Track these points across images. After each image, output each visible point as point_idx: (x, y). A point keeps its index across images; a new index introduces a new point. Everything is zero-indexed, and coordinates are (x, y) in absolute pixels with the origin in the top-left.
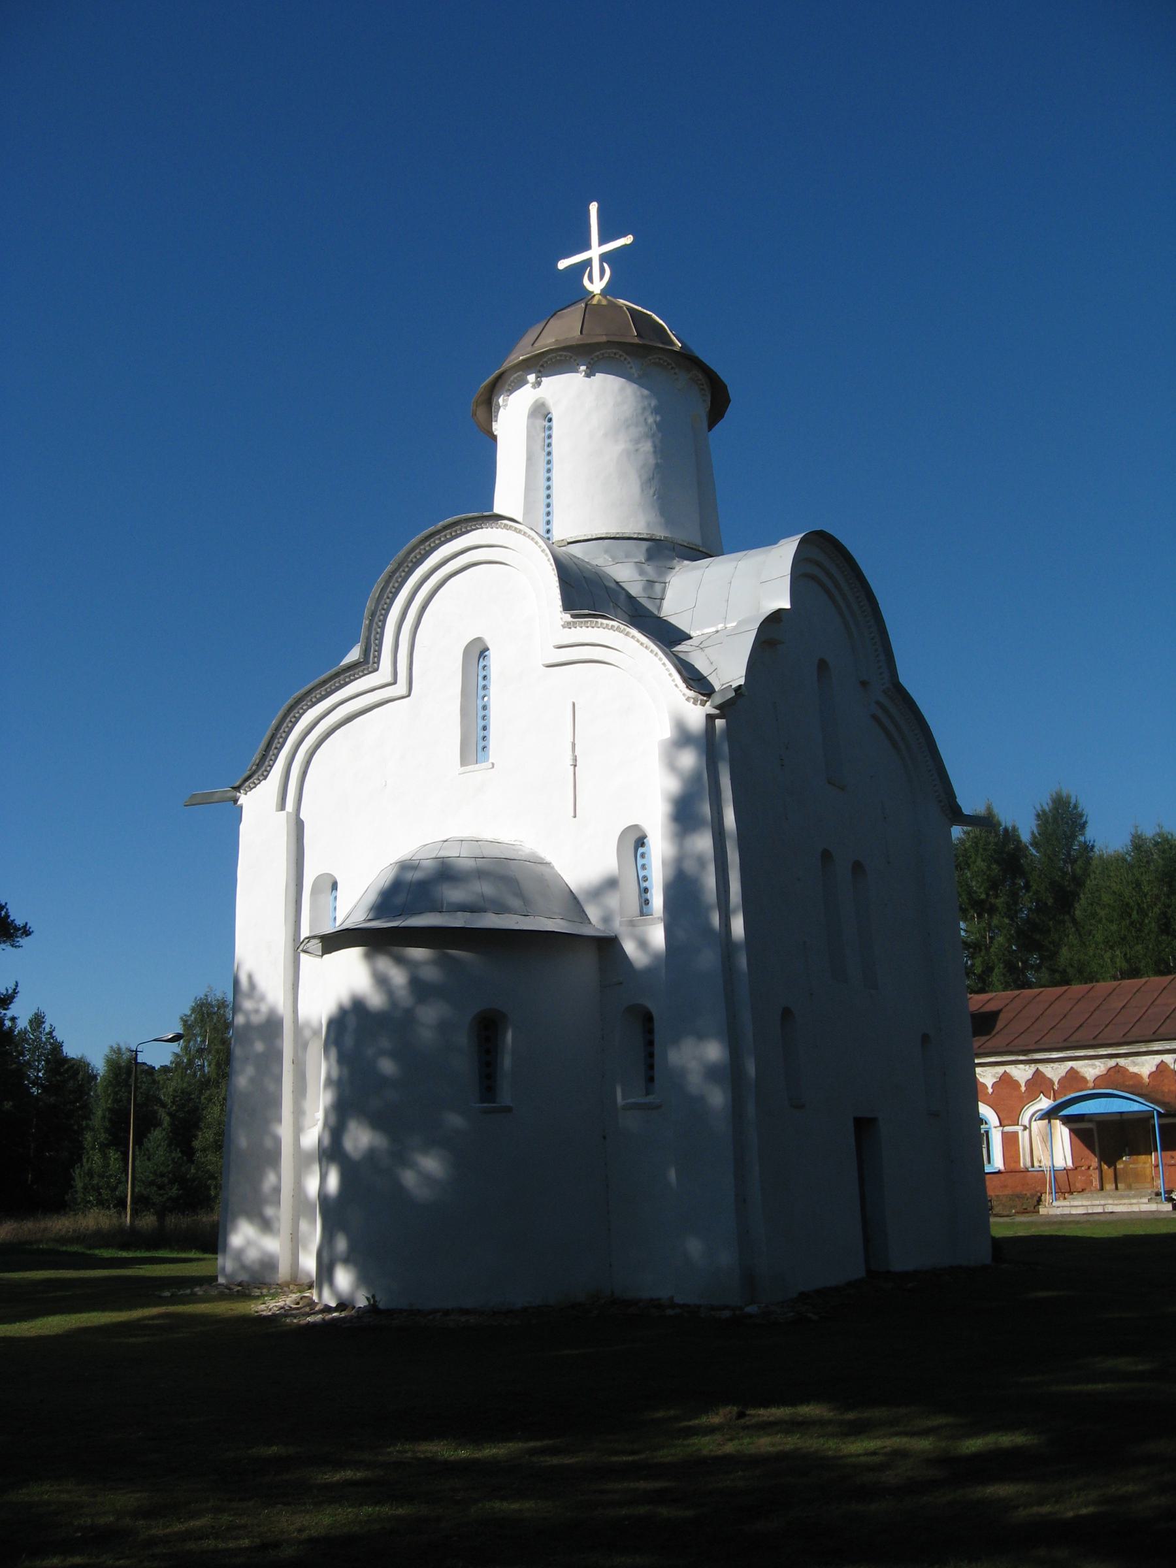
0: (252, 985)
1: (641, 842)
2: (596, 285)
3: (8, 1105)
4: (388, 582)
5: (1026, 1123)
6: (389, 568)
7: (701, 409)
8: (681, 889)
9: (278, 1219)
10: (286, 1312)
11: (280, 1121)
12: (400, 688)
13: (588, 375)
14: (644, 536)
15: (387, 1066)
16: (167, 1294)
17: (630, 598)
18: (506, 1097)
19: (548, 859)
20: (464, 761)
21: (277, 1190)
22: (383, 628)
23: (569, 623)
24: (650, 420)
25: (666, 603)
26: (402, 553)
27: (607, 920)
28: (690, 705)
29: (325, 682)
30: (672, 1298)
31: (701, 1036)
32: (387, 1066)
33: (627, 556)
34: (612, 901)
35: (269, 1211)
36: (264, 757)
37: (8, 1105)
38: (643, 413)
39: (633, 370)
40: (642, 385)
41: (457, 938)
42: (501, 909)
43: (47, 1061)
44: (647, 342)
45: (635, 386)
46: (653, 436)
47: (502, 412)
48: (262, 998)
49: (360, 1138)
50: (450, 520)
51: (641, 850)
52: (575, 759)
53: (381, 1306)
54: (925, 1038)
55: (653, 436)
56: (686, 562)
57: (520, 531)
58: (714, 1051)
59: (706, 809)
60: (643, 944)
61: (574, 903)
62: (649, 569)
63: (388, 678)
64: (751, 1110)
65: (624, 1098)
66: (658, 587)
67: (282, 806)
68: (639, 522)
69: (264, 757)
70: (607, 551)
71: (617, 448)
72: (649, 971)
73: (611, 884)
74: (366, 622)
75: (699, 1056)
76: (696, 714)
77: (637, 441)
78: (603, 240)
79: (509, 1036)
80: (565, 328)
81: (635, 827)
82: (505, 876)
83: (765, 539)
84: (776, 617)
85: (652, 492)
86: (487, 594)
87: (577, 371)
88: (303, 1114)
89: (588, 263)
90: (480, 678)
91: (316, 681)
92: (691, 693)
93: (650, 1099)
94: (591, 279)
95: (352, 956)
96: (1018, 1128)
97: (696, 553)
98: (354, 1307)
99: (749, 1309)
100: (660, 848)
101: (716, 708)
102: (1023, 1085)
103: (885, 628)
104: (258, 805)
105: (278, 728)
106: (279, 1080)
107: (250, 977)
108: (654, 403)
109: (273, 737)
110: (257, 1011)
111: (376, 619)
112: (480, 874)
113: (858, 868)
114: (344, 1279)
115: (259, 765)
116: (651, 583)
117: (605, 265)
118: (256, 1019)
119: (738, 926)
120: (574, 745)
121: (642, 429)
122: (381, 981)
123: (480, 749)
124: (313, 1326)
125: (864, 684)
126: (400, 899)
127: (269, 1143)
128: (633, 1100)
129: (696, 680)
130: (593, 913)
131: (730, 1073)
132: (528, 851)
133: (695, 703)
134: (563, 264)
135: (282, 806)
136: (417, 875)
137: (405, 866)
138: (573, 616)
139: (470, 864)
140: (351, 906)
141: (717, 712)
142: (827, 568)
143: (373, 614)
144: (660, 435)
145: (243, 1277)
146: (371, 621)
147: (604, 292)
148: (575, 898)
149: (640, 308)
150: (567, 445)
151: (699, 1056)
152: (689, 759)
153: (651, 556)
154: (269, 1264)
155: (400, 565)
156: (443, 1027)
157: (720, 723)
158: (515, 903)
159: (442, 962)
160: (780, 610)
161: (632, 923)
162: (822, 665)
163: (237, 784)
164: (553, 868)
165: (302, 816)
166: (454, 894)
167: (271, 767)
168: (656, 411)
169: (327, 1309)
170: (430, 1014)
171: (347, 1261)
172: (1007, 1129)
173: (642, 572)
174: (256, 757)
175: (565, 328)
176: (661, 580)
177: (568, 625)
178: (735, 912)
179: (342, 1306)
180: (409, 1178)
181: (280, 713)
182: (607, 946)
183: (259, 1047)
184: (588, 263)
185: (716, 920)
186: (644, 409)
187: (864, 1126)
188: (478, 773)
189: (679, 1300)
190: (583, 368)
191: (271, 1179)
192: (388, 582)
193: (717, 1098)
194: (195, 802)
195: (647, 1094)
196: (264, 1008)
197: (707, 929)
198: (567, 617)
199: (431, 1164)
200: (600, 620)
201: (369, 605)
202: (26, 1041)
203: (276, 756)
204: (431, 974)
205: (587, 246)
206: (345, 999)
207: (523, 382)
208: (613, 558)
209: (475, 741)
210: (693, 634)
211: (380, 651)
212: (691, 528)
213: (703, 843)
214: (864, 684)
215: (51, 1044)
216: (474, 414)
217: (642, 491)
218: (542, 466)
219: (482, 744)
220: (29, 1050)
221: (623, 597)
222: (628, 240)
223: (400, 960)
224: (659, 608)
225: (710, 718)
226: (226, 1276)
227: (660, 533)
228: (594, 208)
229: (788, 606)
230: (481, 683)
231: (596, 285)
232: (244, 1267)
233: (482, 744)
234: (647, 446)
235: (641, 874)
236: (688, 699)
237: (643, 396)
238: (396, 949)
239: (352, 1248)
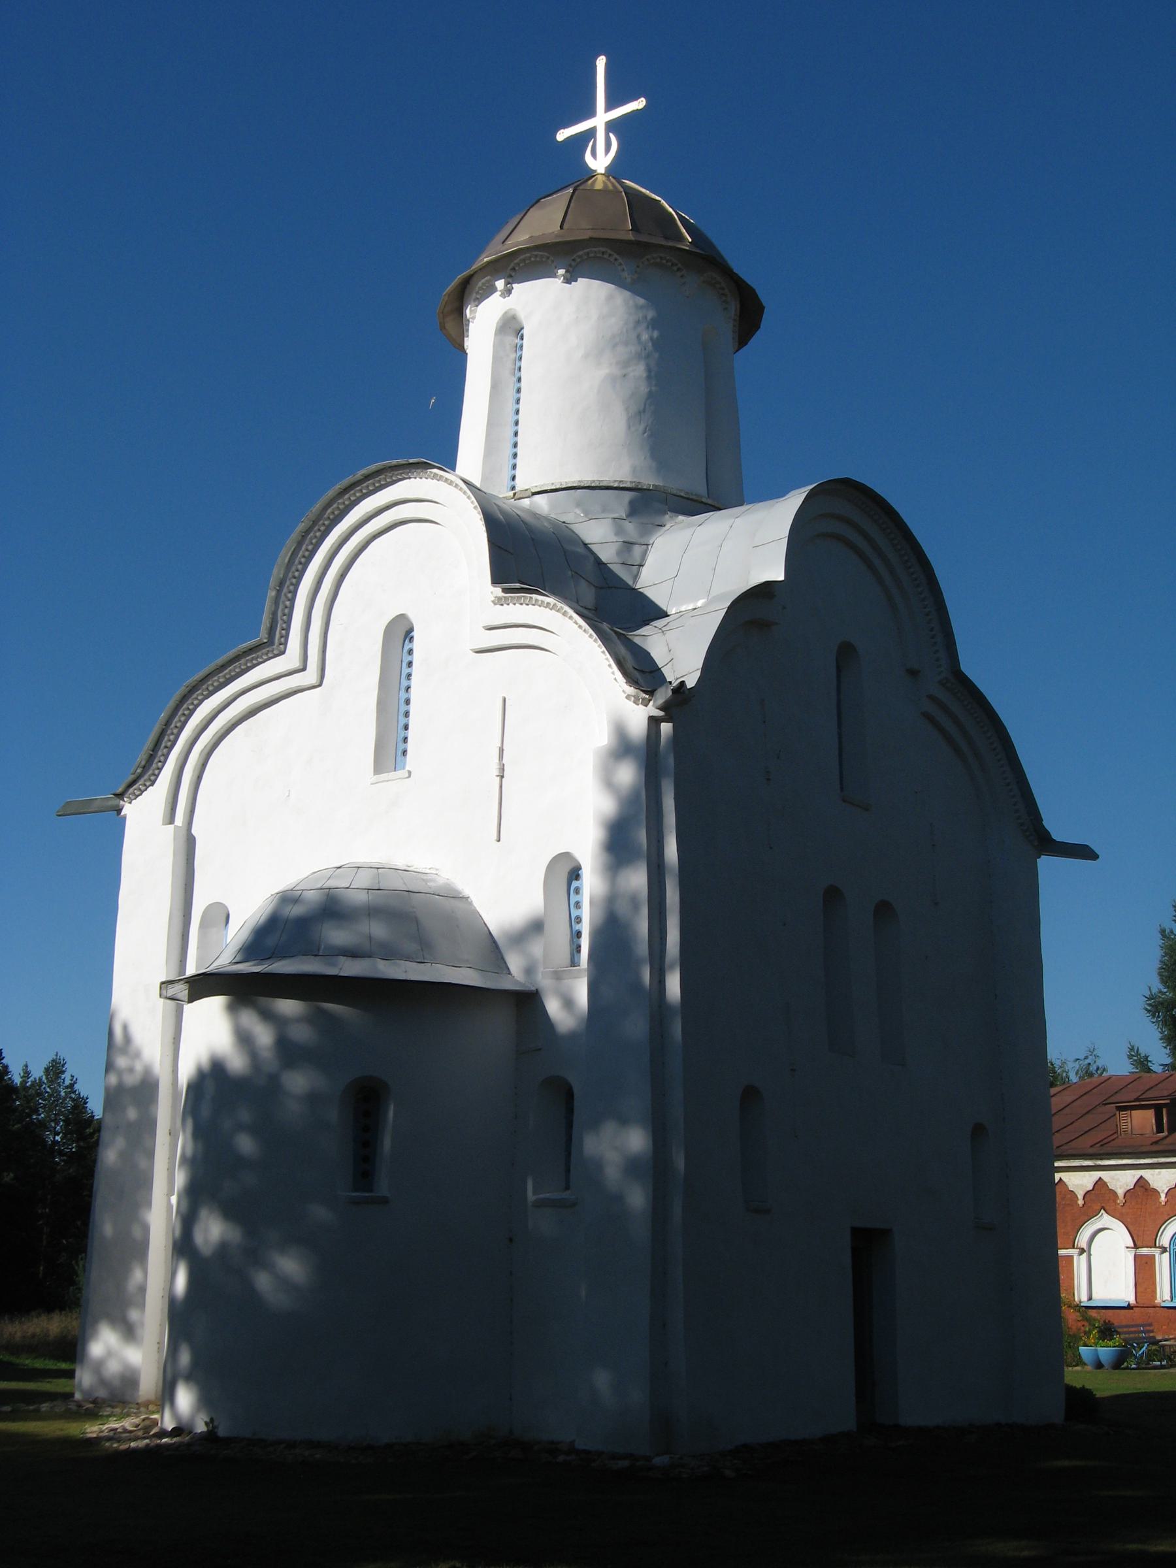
1: (575, 874)
2: (599, 160)
3: (9, 1177)
4: (300, 544)
5: (1084, 1245)
6: (301, 527)
7: (722, 321)
8: (611, 937)
9: (142, 1324)
10: (115, 1436)
11: (149, 1204)
12: (310, 676)
13: (568, 280)
14: (628, 485)
15: (246, 1144)
16: (7, 1408)
17: (600, 564)
18: (383, 1186)
19: (467, 891)
20: (378, 768)
21: (142, 1289)
22: (293, 600)
23: (499, 599)
24: (645, 337)
25: (645, 571)
26: (318, 506)
27: (529, 971)
29: (223, 667)
30: (573, 1442)
31: (624, 1121)
32: (246, 1144)
33: (604, 511)
34: (537, 948)
35: (134, 1315)
36: (151, 758)
37: (9, 1177)
38: (635, 328)
39: (625, 274)
41: (343, 985)
42: (389, 953)
43: (67, 1122)
44: (644, 238)
45: (627, 294)
46: (648, 356)
48: (137, 1055)
49: (213, 1230)
51: (575, 884)
52: (502, 769)
53: (222, 1432)
54: (978, 1130)
56: (681, 518)
57: (451, 483)
58: (636, 1140)
60: (568, 1003)
61: (492, 951)
62: (631, 527)
64: (677, 1211)
65: (534, 1193)
66: (637, 550)
67: (170, 818)
68: (621, 471)
69: (151, 758)
70: (578, 505)
72: (573, 1036)
73: (536, 927)
74: (272, 593)
75: (618, 1144)
76: (637, 716)
77: (625, 364)
78: (611, 105)
79: (391, 1114)
80: (544, 221)
81: (566, 856)
82: (408, 913)
83: (777, 492)
84: (765, 591)
85: (642, 427)
87: (554, 276)
88: (158, 1194)
89: (591, 133)
90: (404, 665)
92: (631, 690)
93: (566, 1195)
94: (594, 154)
95: (213, 1007)
96: (1073, 1252)
98: (190, 1432)
99: (658, 1461)
100: (592, 883)
101: (660, 709)
102: (1080, 1197)
103: (943, 601)
104: (144, 815)
105: (168, 723)
106: (151, 1155)
107: (125, 1028)
108: (651, 314)
109: (162, 734)
110: (131, 1070)
111: (285, 590)
112: (373, 911)
113: (884, 910)
114: (185, 1399)
115: (145, 768)
116: (628, 544)
117: (611, 135)
118: (130, 1080)
119: (673, 985)
120: (501, 750)
121: (634, 348)
122: (243, 1038)
123: (400, 752)
124: (135, 1451)
125: (913, 673)
126: (271, 941)
127: (137, 1232)
128: (548, 1195)
129: (642, 673)
130: (515, 963)
131: (655, 1169)
133: (636, 702)
134: (562, 135)
135: (170, 818)
136: (296, 911)
137: (287, 898)
138: (505, 590)
139: (361, 898)
141: (661, 713)
142: (851, 528)
143: (281, 584)
144: (656, 355)
145: (102, 1393)
146: (279, 592)
147: (611, 171)
148: (495, 942)
150: (546, 372)
151: (618, 1144)
152: (627, 774)
154: (130, 1379)
156: (312, 1099)
157: (666, 728)
158: (411, 947)
159: (317, 1019)
160: (768, 585)
161: (558, 976)
162: (846, 652)
163: (120, 790)
164: (471, 903)
165: (194, 832)
166: (337, 936)
167: (160, 769)
168: (654, 324)
169: (163, 1433)
170: (298, 1082)
171: (189, 1378)
172: (1144, 1251)
173: (619, 531)
174: (142, 758)
175: (544, 221)
176: (643, 541)
177: (499, 601)
178: (672, 967)
179: (177, 1431)
180: (263, 1281)
181: (171, 704)
183: (132, 1114)
184: (591, 133)
185: (646, 975)
186: (638, 322)
187: (868, 1244)
188: (393, 783)
189: (580, 1445)
190: (561, 272)
191: (137, 1275)
192: (300, 544)
193: (637, 1198)
194: (70, 810)
195: (567, 1188)
196: (139, 1067)
197: (637, 986)
198: (498, 591)
199: (291, 1266)
200: (534, 596)
201: (277, 573)
202: (40, 1094)
203: (166, 756)
204: (302, 1034)
205: (590, 112)
206: (205, 1061)
207: (490, 290)
208: (586, 513)
209: (391, 748)
210: (672, 611)
212: (688, 476)
213: (637, 879)
214: (913, 673)
215: (73, 1100)
216: (443, 327)
218: (511, 394)
219: (401, 746)
220: (44, 1107)
221: (592, 559)
222: (639, 104)
223: (267, 1016)
224: (636, 577)
225: (654, 722)
226: (82, 1391)
228: (601, 63)
229: (777, 573)
230: (405, 671)
231: (599, 160)
232: (103, 1382)
233: (401, 746)
234: (639, 370)
235: (574, 913)
236: (628, 697)
237: (639, 308)
238: (264, 1001)
239: (195, 1363)
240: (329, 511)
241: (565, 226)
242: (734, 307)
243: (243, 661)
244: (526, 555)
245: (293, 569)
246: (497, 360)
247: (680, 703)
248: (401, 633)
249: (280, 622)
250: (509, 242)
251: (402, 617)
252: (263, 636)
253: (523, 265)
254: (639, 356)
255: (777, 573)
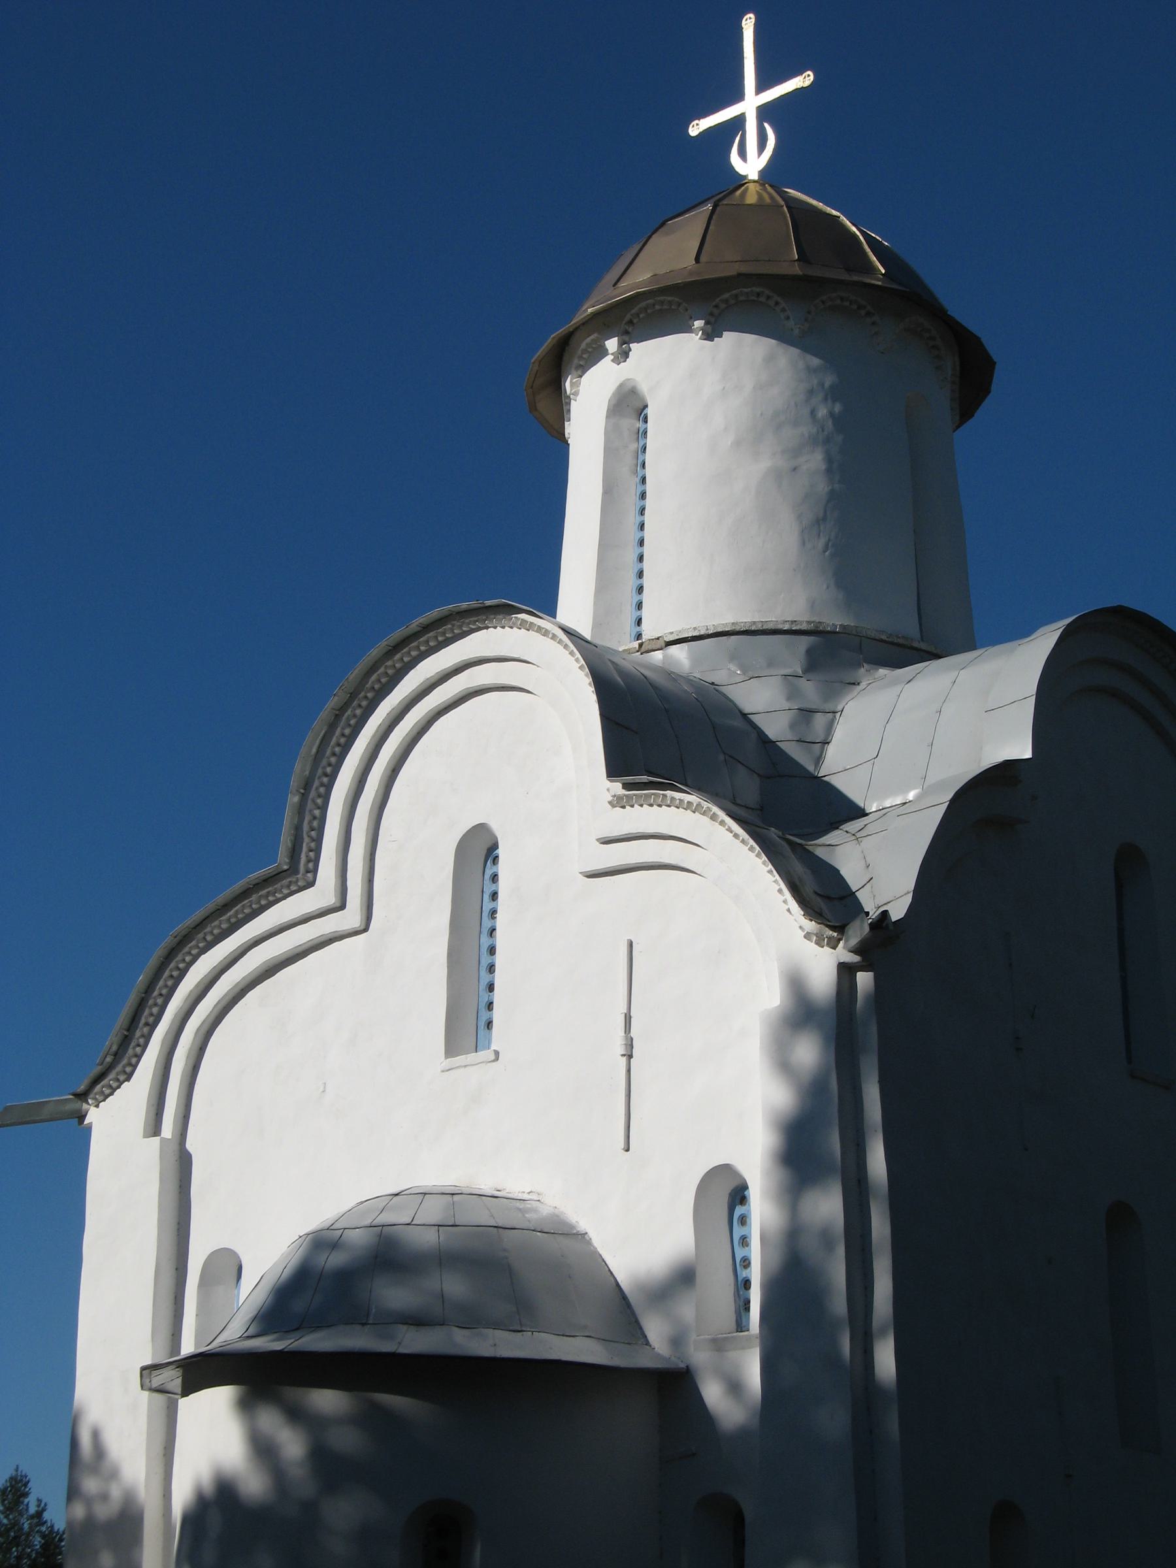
0: (99, 1451)
1: (739, 1195)
2: (750, 163)
4: (332, 727)
6: (333, 702)
8: (793, 1285)
12: (351, 917)
13: (709, 336)
14: (804, 627)
20: (452, 1047)
22: (324, 808)
24: (822, 412)
25: (831, 751)
27: (677, 1341)
28: (811, 946)
33: (771, 664)
34: (687, 1310)
36: (125, 1041)
40: (806, 349)
45: (794, 352)
46: (827, 440)
47: (574, 406)
48: (114, 1474)
50: (435, 613)
52: (630, 1044)
55: (827, 440)
56: (882, 671)
57: (545, 633)
59: (834, 1142)
60: (735, 1387)
61: (622, 1311)
62: (810, 689)
63: (331, 900)
66: (820, 720)
67: (154, 1128)
68: (793, 605)
69: (125, 1041)
70: (733, 658)
71: (759, 466)
72: (742, 1435)
73: (684, 1277)
77: (795, 452)
78: (761, 88)
79: (477, 1554)
82: (498, 1259)
85: (821, 543)
86: (497, 741)
87: (688, 329)
89: (738, 123)
90: (486, 897)
91: (210, 906)
92: (811, 926)
94: (743, 154)
97: (901, 653)
100: (763, 1211)
104: (116, 1123)
107: (96, 1435)
108: (829, 380)
109: (141, 1005)
110: (105, 1497)
111: (313, 794)
112: (446, 1259)
115: (118, 1055)
116: (806, 714)
117: (766, 125)
118: (103, 1512)
120: (628, 1019)
121: (806, 429)
122: (262, 1449)
126: (299, 1305)
129: (826, 899)
130: (656, 1330)
132: (545, 1210)
133: (819, 943)
134: (696, 128)
135: (154, 1128)
136: (335, 1260)
137: (322, 1241)
138: (627, 786)
139: (428, 1239)
140: (227, 1319)
141: (856, 958)
143: (307, 785)
144: (839, 438)
146: (304, 797)
147: (766, 174)
149: (820, 205)
152: (808, 1052)
153: (814, 663)
155: (353, 695)
157: (864, 979)
159: (371, 1419)
161: (719, 1345)
164: (589, 1242)
165: (190, 1146)
166: (394, 1295)
168: (833, 394)
173: (792, 693)
175: (673, 253)
176: (829, 706)
177: (618, 802)
178: (883, 1332)
181: (153, 962)
182: (673, 1387)
184: (738, 123)
185: (845, 1345)
186: (811, 393)
188: (473, 1070)
190: (698, 324)
192: (332, 727)
196: (116, 1492)
198: (617, 787)
200: (669, 793)
201: (300, 768)
204: (347, 1440)
205: (737, 95)
209: (470, 1018)
211: (318, 851)
213: (827, 1206)
215: (44, 1536)
216: (533, 408)
217: (804, 543)
223: (296, 1415)
224: (819, 760)
225: (846, 971)
227: (834, 619)
228: (748, 25)
229: (1028, 754)
231: (750, 163)
234: (815, 460)
236: (808, 936)
237: (811, 370)
238: (294, 1393)
240: (374, 677)
241: (703, 258)
242: (338, 905)
243: (254, 897)
244: (656, 733)
245: (324, 762)
246: (610, 452)
247: (882, 943)
248: (479, 853)
249: (306, 839)
250: (622, 284)
251: (481, 829)
252: (282, 860)
253: (643, 317)
254: (813, 441)
255: (1028, 754)
